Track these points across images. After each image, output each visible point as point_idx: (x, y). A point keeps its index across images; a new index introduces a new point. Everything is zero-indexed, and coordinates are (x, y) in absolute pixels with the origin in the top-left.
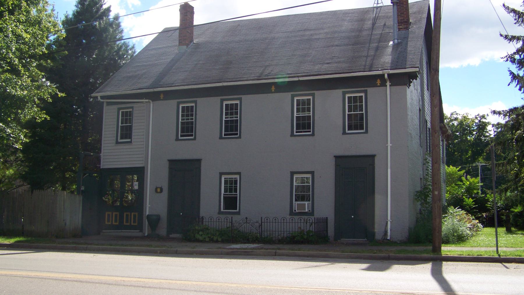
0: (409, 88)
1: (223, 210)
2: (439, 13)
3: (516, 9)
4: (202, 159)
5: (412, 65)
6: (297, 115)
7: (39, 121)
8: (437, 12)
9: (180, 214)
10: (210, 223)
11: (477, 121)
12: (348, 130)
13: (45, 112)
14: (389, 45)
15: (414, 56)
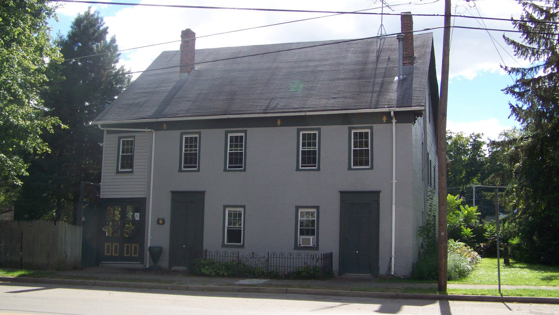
0: (414, 125)
1: (227, 243)
2: (448, 59)
3: (515, 41)
4: (205, 192)
5: (418, 104)
6: (302, 149)
7: (40, 153)
8: (445, 58)
9: (183, 247)
10: (216, 257)
11: (471, 140)
12: (354, 165)
13: (47, 144)
14: (395, 80)
15: (419, 94)
